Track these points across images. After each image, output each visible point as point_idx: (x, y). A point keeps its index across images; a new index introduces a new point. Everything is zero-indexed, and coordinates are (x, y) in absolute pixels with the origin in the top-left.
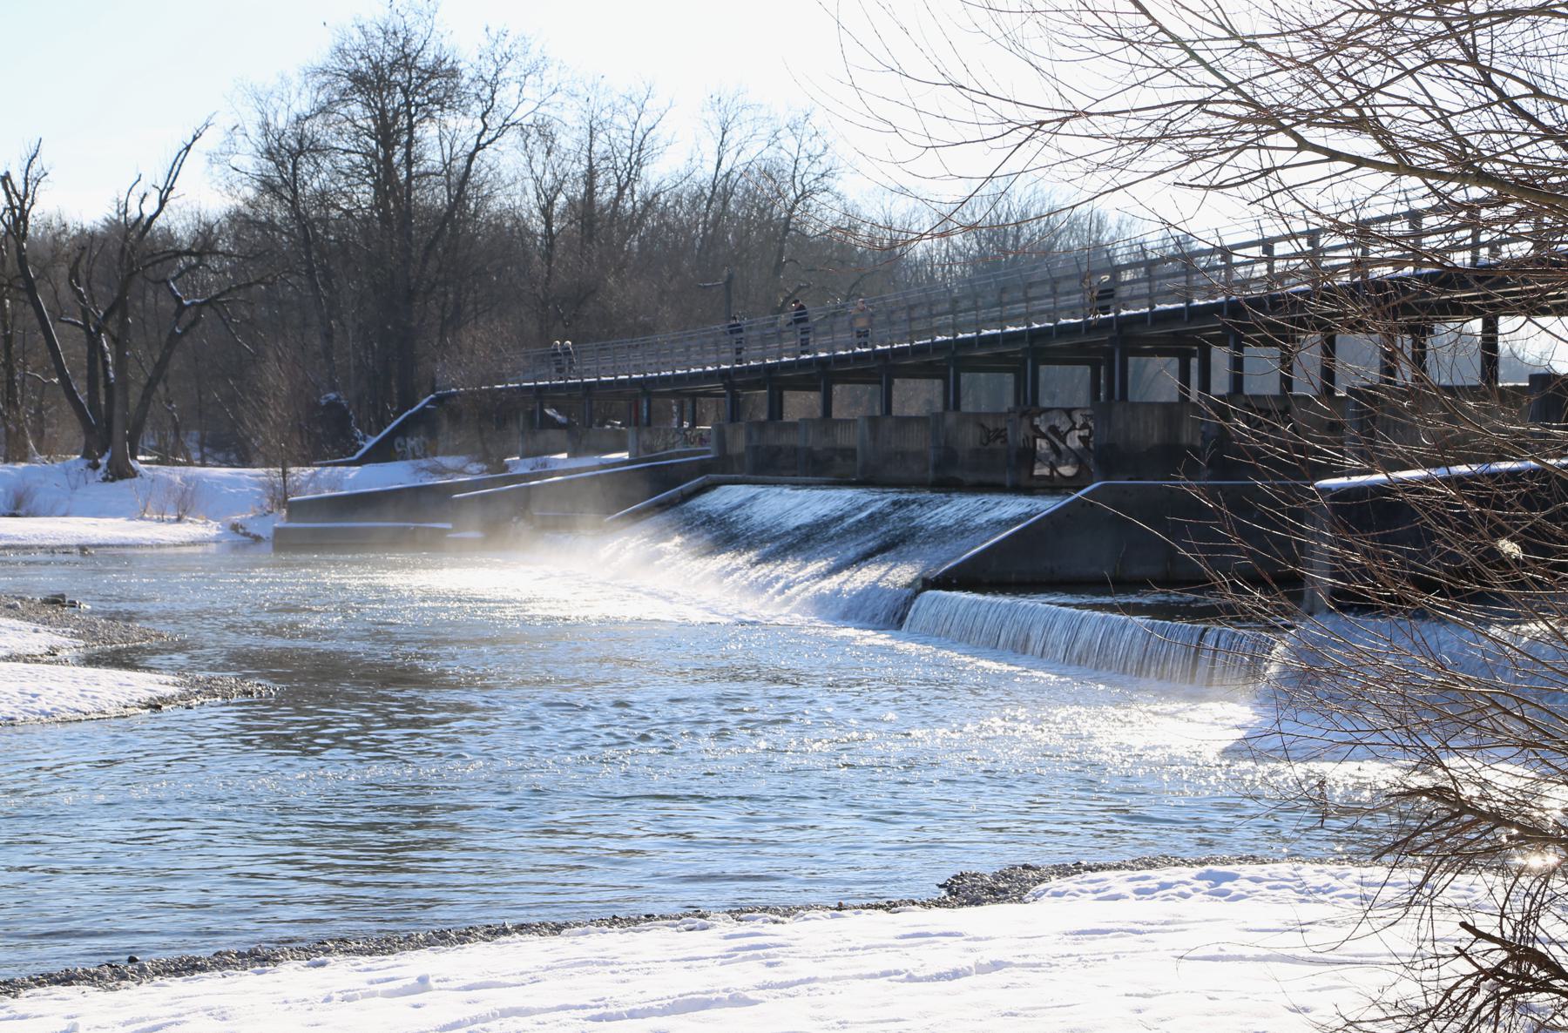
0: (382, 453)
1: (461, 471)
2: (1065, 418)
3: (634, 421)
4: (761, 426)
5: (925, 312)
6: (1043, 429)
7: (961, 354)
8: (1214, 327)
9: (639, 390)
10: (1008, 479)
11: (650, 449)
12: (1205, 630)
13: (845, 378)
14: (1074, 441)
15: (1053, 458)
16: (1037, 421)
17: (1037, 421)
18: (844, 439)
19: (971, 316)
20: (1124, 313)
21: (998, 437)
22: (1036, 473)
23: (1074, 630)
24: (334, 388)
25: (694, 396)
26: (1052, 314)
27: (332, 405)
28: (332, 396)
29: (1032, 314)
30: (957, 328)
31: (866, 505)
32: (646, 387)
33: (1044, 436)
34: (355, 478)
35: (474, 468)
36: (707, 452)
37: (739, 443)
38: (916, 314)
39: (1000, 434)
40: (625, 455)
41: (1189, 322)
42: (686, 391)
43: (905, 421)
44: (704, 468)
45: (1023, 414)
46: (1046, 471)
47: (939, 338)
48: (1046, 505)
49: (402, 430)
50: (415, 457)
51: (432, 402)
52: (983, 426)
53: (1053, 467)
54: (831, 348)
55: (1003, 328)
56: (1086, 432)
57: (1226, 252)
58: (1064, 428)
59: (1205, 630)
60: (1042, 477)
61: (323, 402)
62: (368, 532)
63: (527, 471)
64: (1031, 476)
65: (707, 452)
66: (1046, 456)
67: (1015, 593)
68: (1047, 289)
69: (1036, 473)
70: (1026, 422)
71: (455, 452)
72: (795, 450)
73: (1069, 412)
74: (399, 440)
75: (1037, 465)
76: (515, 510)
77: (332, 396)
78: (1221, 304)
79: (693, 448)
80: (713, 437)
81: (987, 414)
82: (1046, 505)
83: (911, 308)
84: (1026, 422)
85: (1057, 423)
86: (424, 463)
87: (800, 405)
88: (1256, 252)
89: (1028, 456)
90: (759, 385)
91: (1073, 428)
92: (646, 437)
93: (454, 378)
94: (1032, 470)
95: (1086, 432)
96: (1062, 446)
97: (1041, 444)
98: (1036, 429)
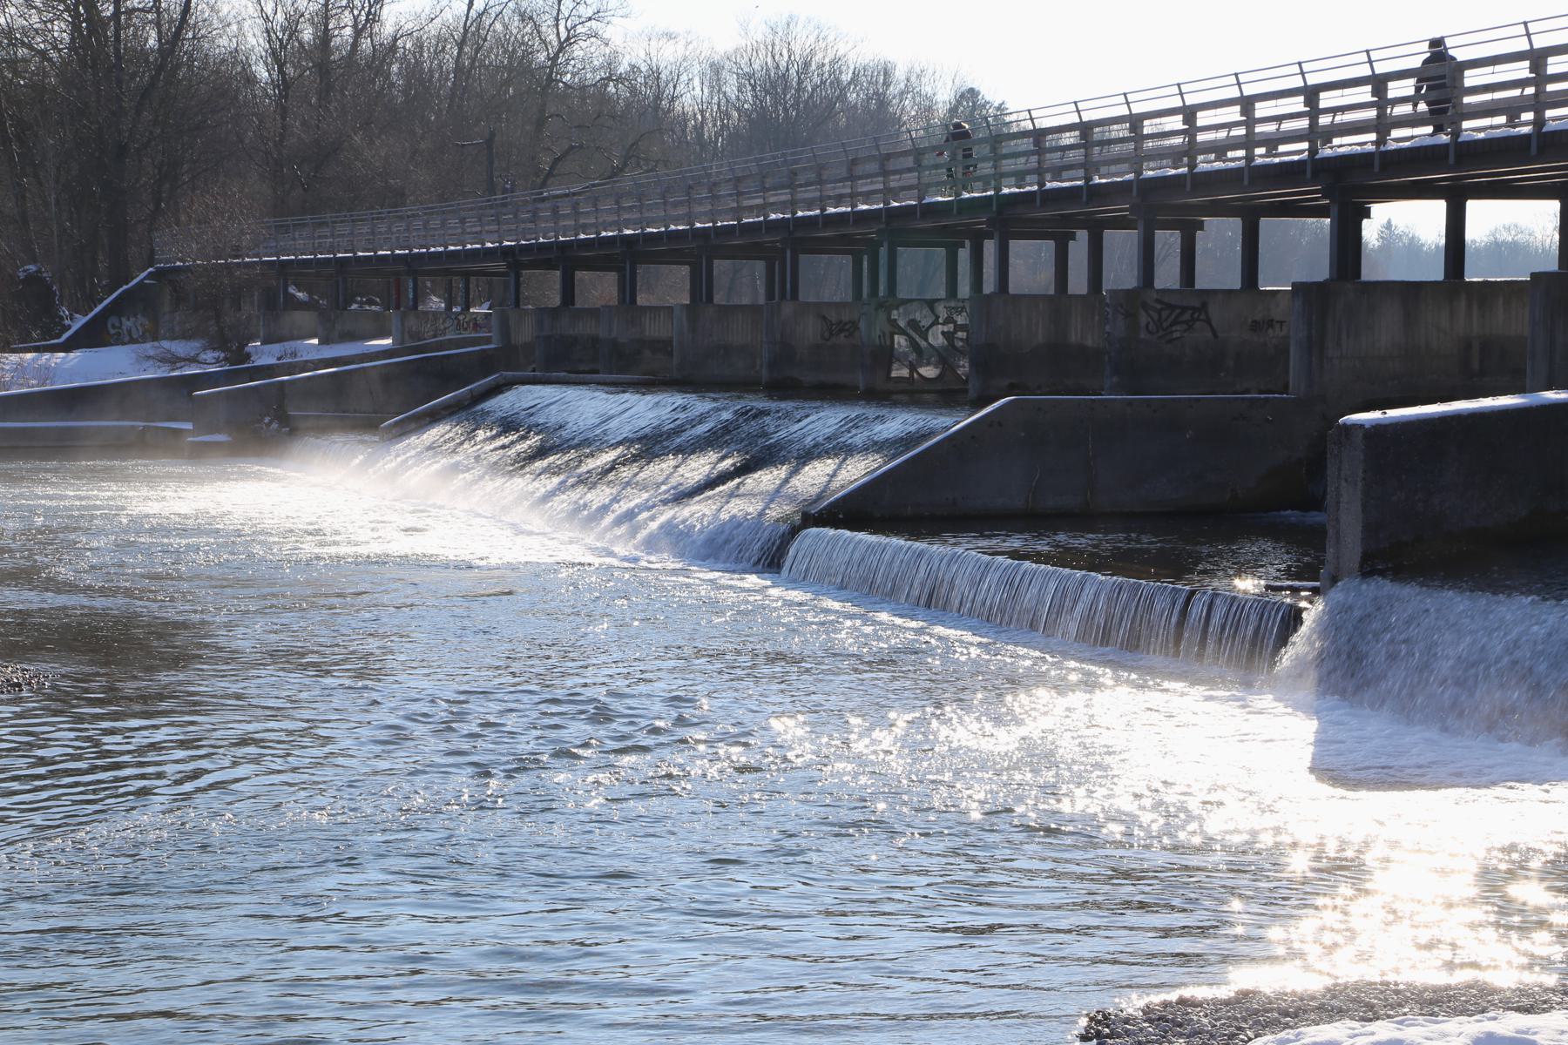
0: (92, 337)
1: (193, 360)
2: (926, 311)
3: (394, 299)
4: (554, 312)
5: (812, 176)
6: (902, 324)
7: (799, 234)
8: (1121, 208)
9: (402, 268)
10: (860, 380)
11: (417, 336)
12: (1193, 593)
13: (590, 265)
14: (936, 338)
15: (913, 357)
16: (895, 314)
17: (895, 314)
18: (655, 329)
19: (911, 178)
20: (966, 195)
21: (841, 331)
22: (894, 374)
23: (1011, 585)
24: (34, 261)
25: (466, 275)
26: (763, 209)
27: (32, 279)
28: (32, 268)
29: (1003, 175)
30: (890, 193)
31: (702, 419)
32: (413, 266)
33: (903, 332)
34: (70, 367)
35: (209, 356)
36: (488, 340)
37: (525, 332)
38: (891, 165)
39: (850, 328)
40: (388, 342)
41: (1087, 204)
42: (456, 272)
43: (728, 311)
44: (486, 363)
45: (880, 306)
46: (905, 373)
47: (773, 216)
48: (958, 422)
49: (116, 309)
50: (133, 341)
51: (150, 276)
52: (824, 318)
53: (913, 368)
54: (737, 212)
55: (854, 206)
56: (950, 327)
57: (1135, 121)
58: (925, 323)
59: (1193, 593)
60: (900, 379)
61: (22, 275)
62: (112, 468)
63: (272, 361)
64: (889, 378)
65: (488, 340)
66: (906, 355)
67: (915, 535)
68: (909, 162)
69: (894, 374)
70: (882, 316)
71: (186, 336)
72: (595, 340)
73: (931, 304)
74: (113, 320)
75: (895, 366)
76: (267, 418)
77: (32, 268)
78: (1130, 182)
79: (466, 335)
80: (494, 322)
81: (829, 304)
82: (958, 422)
83: (739, 180)
84: (882, 316)
85: (918, 316)
86: (149, 348)
87: (599, 288)
88: (1364, 94)
89: (886, 356)
90: (549, 265)
91: (935, 323)
92: (412, 322)
93: (180, 249)
94: (889, 372)
95: (950, 327)
96: (923, 344)
97: (900, 341)
98: (894, 323)
